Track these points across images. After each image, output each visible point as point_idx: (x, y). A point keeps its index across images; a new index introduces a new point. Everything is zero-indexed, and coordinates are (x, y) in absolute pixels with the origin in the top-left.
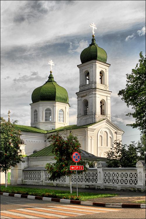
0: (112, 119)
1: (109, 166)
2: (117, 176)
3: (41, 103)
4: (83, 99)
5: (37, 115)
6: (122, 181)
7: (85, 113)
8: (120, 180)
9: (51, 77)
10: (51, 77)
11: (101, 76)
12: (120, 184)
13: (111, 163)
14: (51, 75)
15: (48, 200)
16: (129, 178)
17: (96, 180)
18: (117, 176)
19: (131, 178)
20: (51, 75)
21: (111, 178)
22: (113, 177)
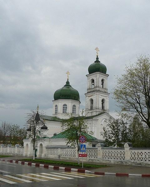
0: (90, 109)
1: (105, 146)
2: (111, 153)
3: (60, 101)
4: (90, 98)
5: (57, 109)
6: (121, 157)
7: (91, 108)
8: (119, 157)
9: (68, 83)
10: (68, 83)
11: (103, 83)
12: (113, 159)
13: (107, 144)
14: (68, 81)
15: (63, 169)
16: (119, 155)
17: (96, 156)
18: (111, 153)
19: (121, 155)
20: (68, 81)
21: (113, 155)
22: (131, 160)
